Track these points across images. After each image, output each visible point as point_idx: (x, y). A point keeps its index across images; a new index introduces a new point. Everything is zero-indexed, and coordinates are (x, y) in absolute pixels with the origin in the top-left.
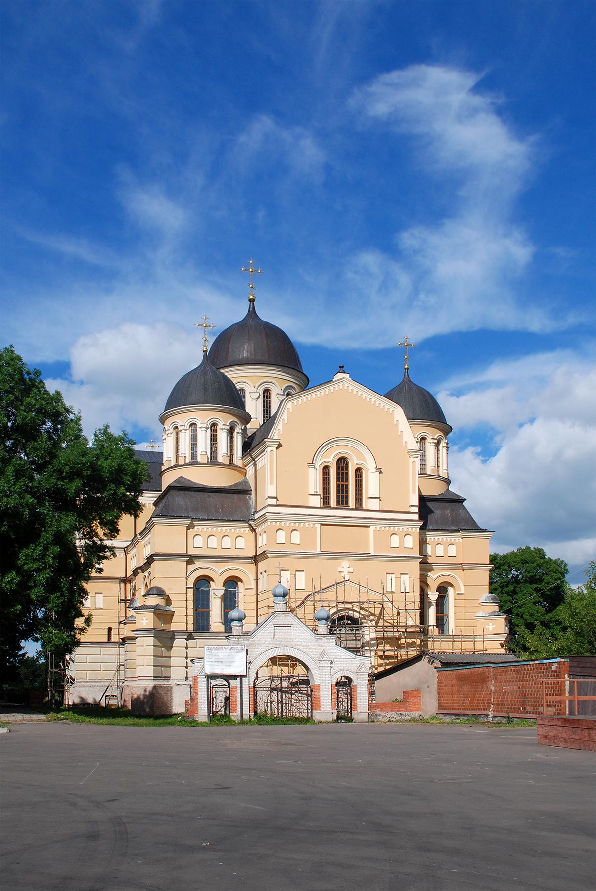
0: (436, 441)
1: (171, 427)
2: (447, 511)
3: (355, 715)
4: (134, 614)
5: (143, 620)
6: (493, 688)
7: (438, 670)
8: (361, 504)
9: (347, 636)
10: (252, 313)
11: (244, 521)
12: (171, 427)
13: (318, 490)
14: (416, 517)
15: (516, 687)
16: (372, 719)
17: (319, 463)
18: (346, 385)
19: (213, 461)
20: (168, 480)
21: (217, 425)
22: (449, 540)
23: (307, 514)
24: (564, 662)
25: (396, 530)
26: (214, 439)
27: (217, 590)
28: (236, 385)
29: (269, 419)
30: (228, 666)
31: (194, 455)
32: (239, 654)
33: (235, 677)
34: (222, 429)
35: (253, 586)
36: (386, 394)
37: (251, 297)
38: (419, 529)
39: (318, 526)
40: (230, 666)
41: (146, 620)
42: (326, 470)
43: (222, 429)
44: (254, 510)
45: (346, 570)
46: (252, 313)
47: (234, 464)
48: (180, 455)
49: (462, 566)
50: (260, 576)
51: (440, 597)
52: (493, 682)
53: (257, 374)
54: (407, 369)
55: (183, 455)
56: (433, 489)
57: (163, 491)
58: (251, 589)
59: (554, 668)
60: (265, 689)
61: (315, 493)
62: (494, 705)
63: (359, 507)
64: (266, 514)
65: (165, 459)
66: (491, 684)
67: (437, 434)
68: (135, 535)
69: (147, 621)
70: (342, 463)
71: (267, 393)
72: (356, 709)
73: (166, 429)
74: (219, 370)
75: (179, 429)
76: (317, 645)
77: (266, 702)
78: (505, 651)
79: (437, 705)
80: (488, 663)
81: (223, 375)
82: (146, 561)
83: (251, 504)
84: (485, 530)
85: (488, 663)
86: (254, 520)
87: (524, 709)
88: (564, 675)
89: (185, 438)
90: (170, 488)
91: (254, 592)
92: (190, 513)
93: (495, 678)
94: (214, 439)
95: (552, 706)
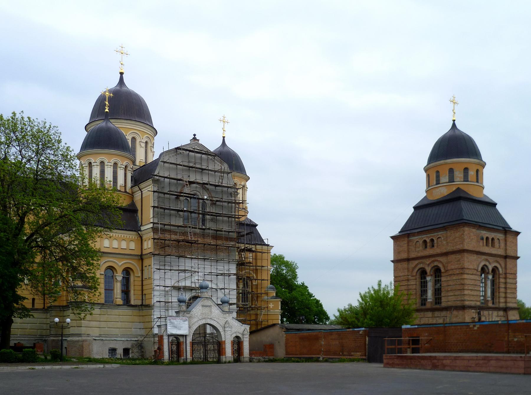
7: (286, 333)
9: (161, 310)
11: (135, 231)
15: (338, 343)
27: (119, 276)
30: (179, 329)
32: (185, 322)
33: (182, 336)
35: (140, 275)
40: (180, 329)
44: (140, 224)
58: (139, 277)
59: (361, 333)
62: (323, 352)
67: (124, 162)
76: (223, 318)
79: (284, 352)
91: (141, 279)
93: (325, 338)
95: (359, 352)
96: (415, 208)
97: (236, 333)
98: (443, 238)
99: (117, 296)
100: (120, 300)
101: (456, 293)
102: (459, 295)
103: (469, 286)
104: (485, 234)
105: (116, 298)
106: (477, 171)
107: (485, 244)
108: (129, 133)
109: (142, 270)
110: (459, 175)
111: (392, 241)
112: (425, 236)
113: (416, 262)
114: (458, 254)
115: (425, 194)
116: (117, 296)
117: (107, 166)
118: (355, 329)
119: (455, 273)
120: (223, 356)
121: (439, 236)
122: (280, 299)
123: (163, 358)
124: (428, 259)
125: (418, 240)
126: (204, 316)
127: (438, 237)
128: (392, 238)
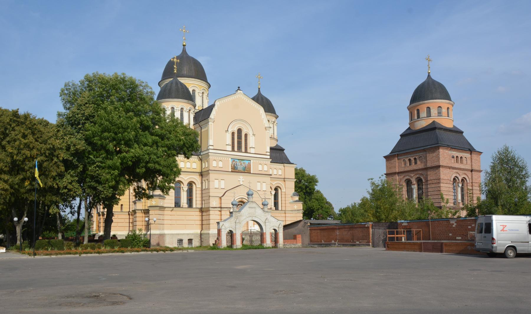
5: (153, 202)
6: (338, 234)
10: (184, 51)
13: (230, 143)
14: (269, 157)
17: (230, 130)
21: (184, 109)
22: (279, 167)
25: (261, 162)
34: (185, 111)
37: (184, 44)
39: (230, 159)
42: (233, 134)
43: (185, 111)
46: (184, 51)
49: (284, 179)
50: (204, 182)
51: (275, 193)
53: (191, 83)
54: (260, 88)
63: (246, 152)
69: (155, 202)
70: (240, 131)
81: (182, 84)
86: (201, 155)
87: (353, 241)
95: (365, 240)
96: (400, 135)
97: (273, 226)
98: (423, 157)
101: (435, 197)
102: (437, 199)
103: (444, 191)
104: (455, 153)
105: (183, 203)
106: (448, 108)
107: (455, 161)
110: (434, 112)
111: (385, 160)
112: (409, 156)
113: (404, 174)
114: (435, 169)
115: (408, 126)
116: (183, 201)
118: (362, 224)
119: (433, 183)
121: (420, 156)
123: (222, 245)
124: (412, 173)
125: (404, 159)
127: (419, 156)
128: (385, 157)
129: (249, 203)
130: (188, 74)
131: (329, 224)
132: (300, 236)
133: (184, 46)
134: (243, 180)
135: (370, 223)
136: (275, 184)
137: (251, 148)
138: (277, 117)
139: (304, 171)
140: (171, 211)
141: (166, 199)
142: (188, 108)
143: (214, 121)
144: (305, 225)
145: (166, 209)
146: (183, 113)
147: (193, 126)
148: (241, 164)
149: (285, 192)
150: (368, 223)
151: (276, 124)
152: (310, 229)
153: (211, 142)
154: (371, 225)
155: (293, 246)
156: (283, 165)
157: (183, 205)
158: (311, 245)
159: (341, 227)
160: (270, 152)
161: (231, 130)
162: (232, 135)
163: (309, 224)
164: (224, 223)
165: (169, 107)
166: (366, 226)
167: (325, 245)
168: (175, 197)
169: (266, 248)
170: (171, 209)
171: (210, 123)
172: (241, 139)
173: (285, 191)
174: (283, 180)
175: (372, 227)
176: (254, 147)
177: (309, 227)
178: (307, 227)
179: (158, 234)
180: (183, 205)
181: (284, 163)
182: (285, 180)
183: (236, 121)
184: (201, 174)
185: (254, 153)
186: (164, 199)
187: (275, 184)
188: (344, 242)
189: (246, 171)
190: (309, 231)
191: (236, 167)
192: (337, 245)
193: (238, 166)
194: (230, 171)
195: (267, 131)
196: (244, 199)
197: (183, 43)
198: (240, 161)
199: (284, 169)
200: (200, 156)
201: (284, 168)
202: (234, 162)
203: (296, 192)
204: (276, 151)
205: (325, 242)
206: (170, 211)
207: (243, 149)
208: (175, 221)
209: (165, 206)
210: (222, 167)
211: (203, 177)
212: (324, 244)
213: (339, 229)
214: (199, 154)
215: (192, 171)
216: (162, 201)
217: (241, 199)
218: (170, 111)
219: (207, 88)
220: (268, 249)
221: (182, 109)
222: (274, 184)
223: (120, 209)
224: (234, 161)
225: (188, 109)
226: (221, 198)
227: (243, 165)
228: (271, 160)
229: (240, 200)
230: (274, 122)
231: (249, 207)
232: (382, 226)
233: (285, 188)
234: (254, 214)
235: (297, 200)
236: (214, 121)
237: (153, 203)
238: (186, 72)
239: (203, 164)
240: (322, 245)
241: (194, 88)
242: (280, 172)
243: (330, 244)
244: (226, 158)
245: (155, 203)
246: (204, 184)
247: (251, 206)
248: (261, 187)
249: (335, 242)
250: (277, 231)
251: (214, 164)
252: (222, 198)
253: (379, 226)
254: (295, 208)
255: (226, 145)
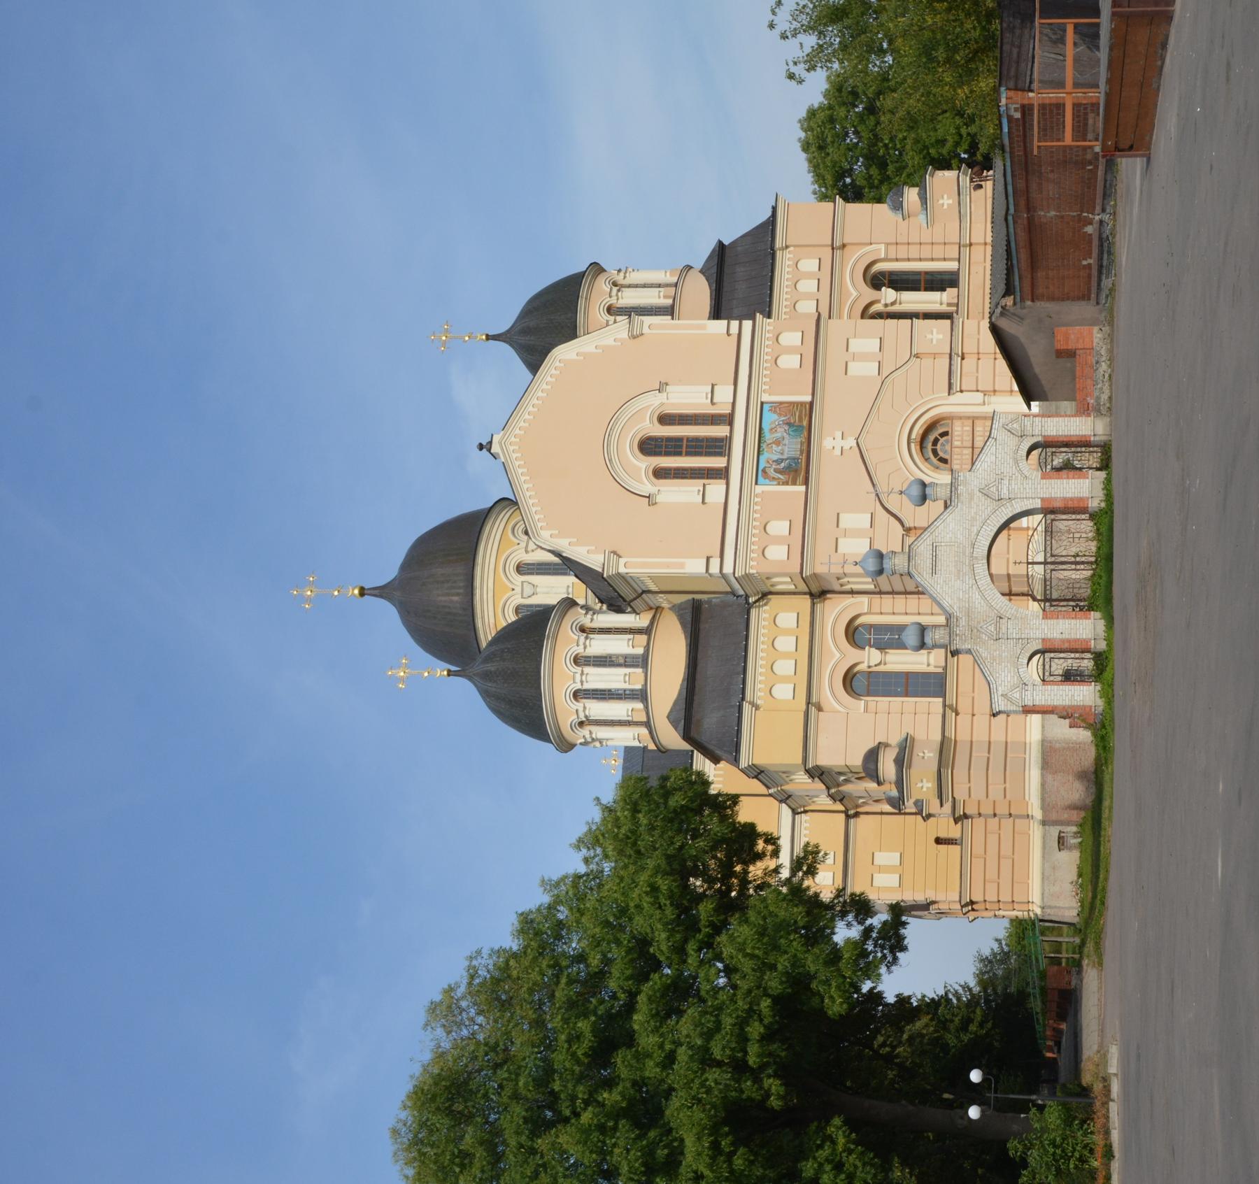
0: (615, 289)
1: (571, 705)
2: (739, 273)
3: (1101, 438)
4: (912, 801)
5: (922, 787)
6: (1053, 213)
8: (720, 416)
10: (382, 592)
11: (748, 613)
12: (571, 705)
14: (747, 324)
16: (1108, 410)
18: (513, 439)
19: (643, 662)
20: (672, 739)
21: (577, 655)
22: (790, 269)
23: (738, 507)
24: (1007, 98)
26: (604, 661)
27: (870, 658)
28: (510, 622)
29: (567, 565)
31: (627, 661)
34: (585, 648)
35: (864, 599)
36: (531, 372)
37: (356, 592)
38: (768, 320)
39: (759, 489)
41: (922, 781)
42: (660, 473)
43: (585, 648)
44: (731, 597)
45: (839, 443)
46: (382, 592)
47: (648, 627)
48: (630, 719)
49: (838, 247)
50: (848, 587)
52: (1042, 213)
53: (491, 585)
54: (487, 335)
55: (630, 714)
56: (699, 291)
57: (692, 748)
60: (1048, 543)
61: (701, 493)
64: (736, 575)
65: (636, 744)
66: (1045, 216)
68: (770, 795)
69: (925, 780)
70: (649, 446)
71: (522, 569)
72: (1087, 641)
73: (583, 740)
74: (482, 649)
75: (584, 719)
77: (1071, 540)
78: (988, 182)
80: (1006, 220)
81: (491, 644)
82: (816, 779)
83: (718, 600)
84: (774, 209)
85: (1006, 220)
87: (1090, 163)
88: (1029, 98)
89: (598, 709)
90: (687, 737)
92: (733, 704)
94: (604, 661)
97: (1016, 462)
99: (923, 664)
100: (932, 656)
105: (928, 665)
108: (509, 584)
109: (852, 592)
116: (923, 664)
117: (585, 683)
120: (1090, 505)
122: (927, 176)
123: (1091, 707)
126: (966, 569)
129: (913, 571)
130: (461, 591)
131: (1008, 242)
132: (1060, 332)
133: (363, 592)
134: (839, 434)
135: (1003, 101)
136: (856, 292)
137: (715, 401)
138: (597, 269)
139: (812, 113)
140: (957, 714)
141: (911, 732)
142: (574, 636)
143: (615, 553)
144: (1014, 314)
145: (950, 733)
146: (594, 657)
147: (642, 615)
148: (778, 442)
149: (887, 244)
150: (1002, 109)
151: (622, 274)
152: (1033, 301)
153: (695, 566)
154: (1011, 93)
155: (1104, 366)
156: (779, 254)
157: (935, 667)
158: (1103, 296)
159: (1022, 202)
160: (729, 318)
161: (648, 483)
162: (665, 478)
163: (1009, 301)
164: (1000, 693)
165: (575, 708)
166: (1018, 115)
167: (1105, 256)
168: (907, 695)
169: (1109, 497)
170: (951, 715)
171: (622, 570)
172: (678, 440)
173: (883, 247)
174: (838, 253)
175: (1023, 90)
176: (709, 388)
177: (1022, 300)
178: (1024, 308)
179: (1043, 776)
180: (935, 667)
181: (772, 248)
182: (838, 243)
183: (610, 460)
184: (819, 593)
185: (733, 387)
186: (913, 740)
187: (856, 289)
188: (1095, 195)
189: (805, 423)
190: (1042, 303)
191: (789, 467)
192: (1106, 217)
193: (785, 456)
194: (803, 488)
195: (646, 331)
196: (913, 436)
197: (355, 595)
198: (764, 446)
199: (795, 246)
200: (751, 600)
201: (791, 249)
202: (771, 472)
203: (888, 200)
204: (726, 278)
205: (1091, 254)
206: (958, 717)
207: (720, 431)
208: (990, 787)
209: (938, 738)
210: (819, 280)
211: (830, 588)
212: (1100, 258)
213: (1029, 208)
214: (742, 601)
215: (807, 630)
216: (918, 753)
217: (913, 445)
218: (587, 705)
219: (512, 511)
220: (1115, 493)
221: (577, 660)
222: (855, 294)
223: (950, 846)
224: (764, 471)
225: (577, 638)
226: (908, 530)
227: (780, 433)
228: (758, 314)
229: (918, 447)
230: (615, 284)
231: (934, 571)
232: (1020, 47)
233: (871, 244)
234: (964, 553)
235: (919, 194)
236: (615, 553)
237: (928, 788)
238: (455, 598)
239: (780, 588)
240: (1105, 263)
241: (513, 573)
242: (809, 265)
243: (1100, 239)
244: (755, 512)
245: (928, 781)
246: (855, 587)
247: (929, 561)
248: (864, 357)
249: (1091, 223)
250: (1038, 442)
251: (777, 553)
252: (907, 525)
253: (1018, 62)
254: (938, 340)
255: (703, 502)
